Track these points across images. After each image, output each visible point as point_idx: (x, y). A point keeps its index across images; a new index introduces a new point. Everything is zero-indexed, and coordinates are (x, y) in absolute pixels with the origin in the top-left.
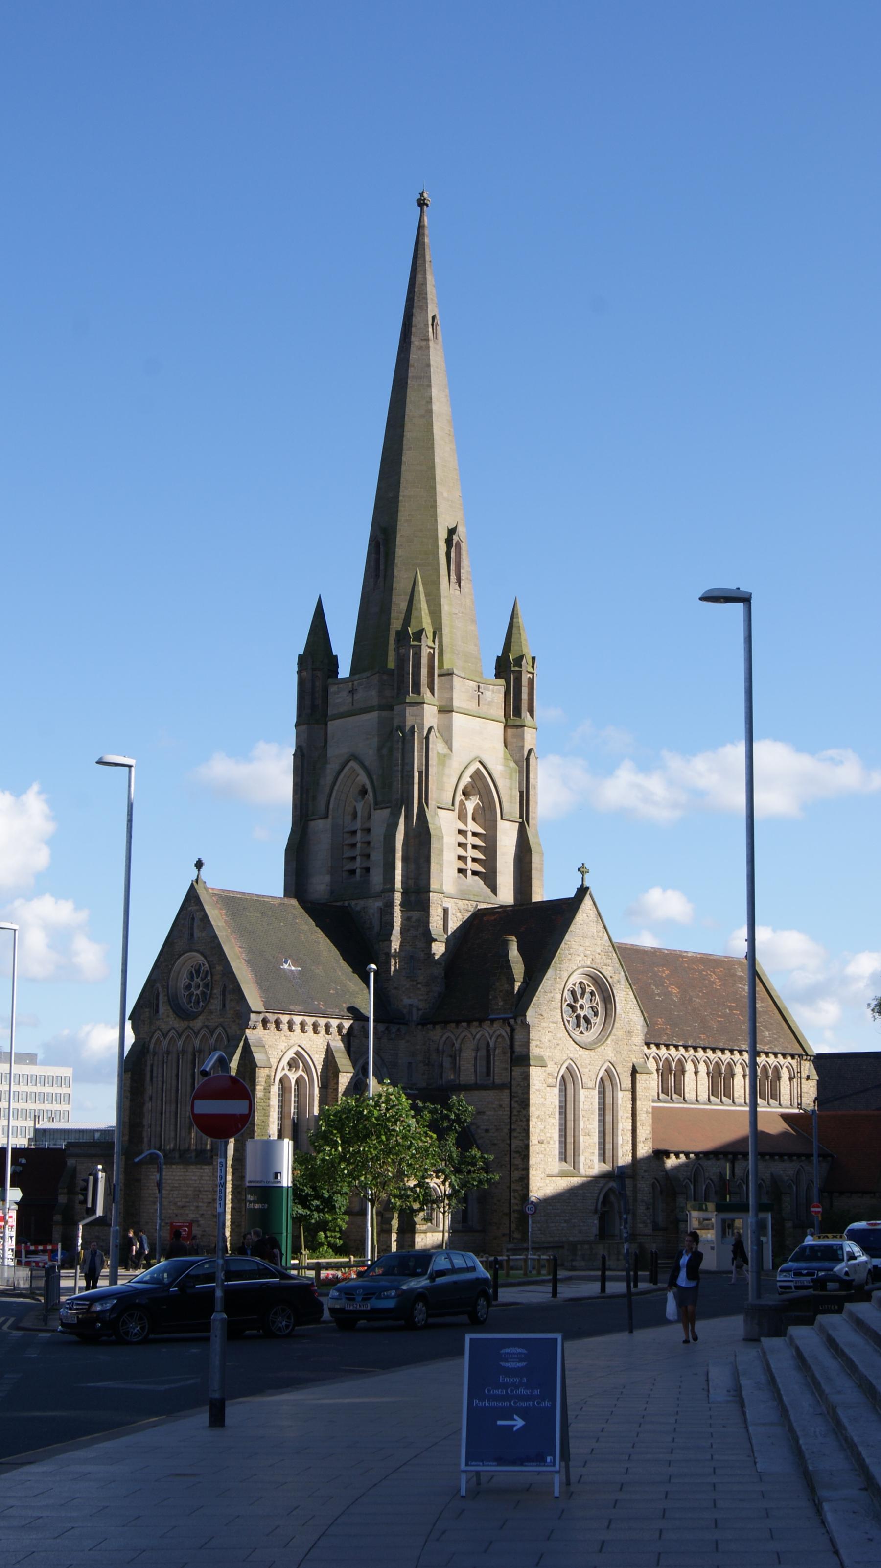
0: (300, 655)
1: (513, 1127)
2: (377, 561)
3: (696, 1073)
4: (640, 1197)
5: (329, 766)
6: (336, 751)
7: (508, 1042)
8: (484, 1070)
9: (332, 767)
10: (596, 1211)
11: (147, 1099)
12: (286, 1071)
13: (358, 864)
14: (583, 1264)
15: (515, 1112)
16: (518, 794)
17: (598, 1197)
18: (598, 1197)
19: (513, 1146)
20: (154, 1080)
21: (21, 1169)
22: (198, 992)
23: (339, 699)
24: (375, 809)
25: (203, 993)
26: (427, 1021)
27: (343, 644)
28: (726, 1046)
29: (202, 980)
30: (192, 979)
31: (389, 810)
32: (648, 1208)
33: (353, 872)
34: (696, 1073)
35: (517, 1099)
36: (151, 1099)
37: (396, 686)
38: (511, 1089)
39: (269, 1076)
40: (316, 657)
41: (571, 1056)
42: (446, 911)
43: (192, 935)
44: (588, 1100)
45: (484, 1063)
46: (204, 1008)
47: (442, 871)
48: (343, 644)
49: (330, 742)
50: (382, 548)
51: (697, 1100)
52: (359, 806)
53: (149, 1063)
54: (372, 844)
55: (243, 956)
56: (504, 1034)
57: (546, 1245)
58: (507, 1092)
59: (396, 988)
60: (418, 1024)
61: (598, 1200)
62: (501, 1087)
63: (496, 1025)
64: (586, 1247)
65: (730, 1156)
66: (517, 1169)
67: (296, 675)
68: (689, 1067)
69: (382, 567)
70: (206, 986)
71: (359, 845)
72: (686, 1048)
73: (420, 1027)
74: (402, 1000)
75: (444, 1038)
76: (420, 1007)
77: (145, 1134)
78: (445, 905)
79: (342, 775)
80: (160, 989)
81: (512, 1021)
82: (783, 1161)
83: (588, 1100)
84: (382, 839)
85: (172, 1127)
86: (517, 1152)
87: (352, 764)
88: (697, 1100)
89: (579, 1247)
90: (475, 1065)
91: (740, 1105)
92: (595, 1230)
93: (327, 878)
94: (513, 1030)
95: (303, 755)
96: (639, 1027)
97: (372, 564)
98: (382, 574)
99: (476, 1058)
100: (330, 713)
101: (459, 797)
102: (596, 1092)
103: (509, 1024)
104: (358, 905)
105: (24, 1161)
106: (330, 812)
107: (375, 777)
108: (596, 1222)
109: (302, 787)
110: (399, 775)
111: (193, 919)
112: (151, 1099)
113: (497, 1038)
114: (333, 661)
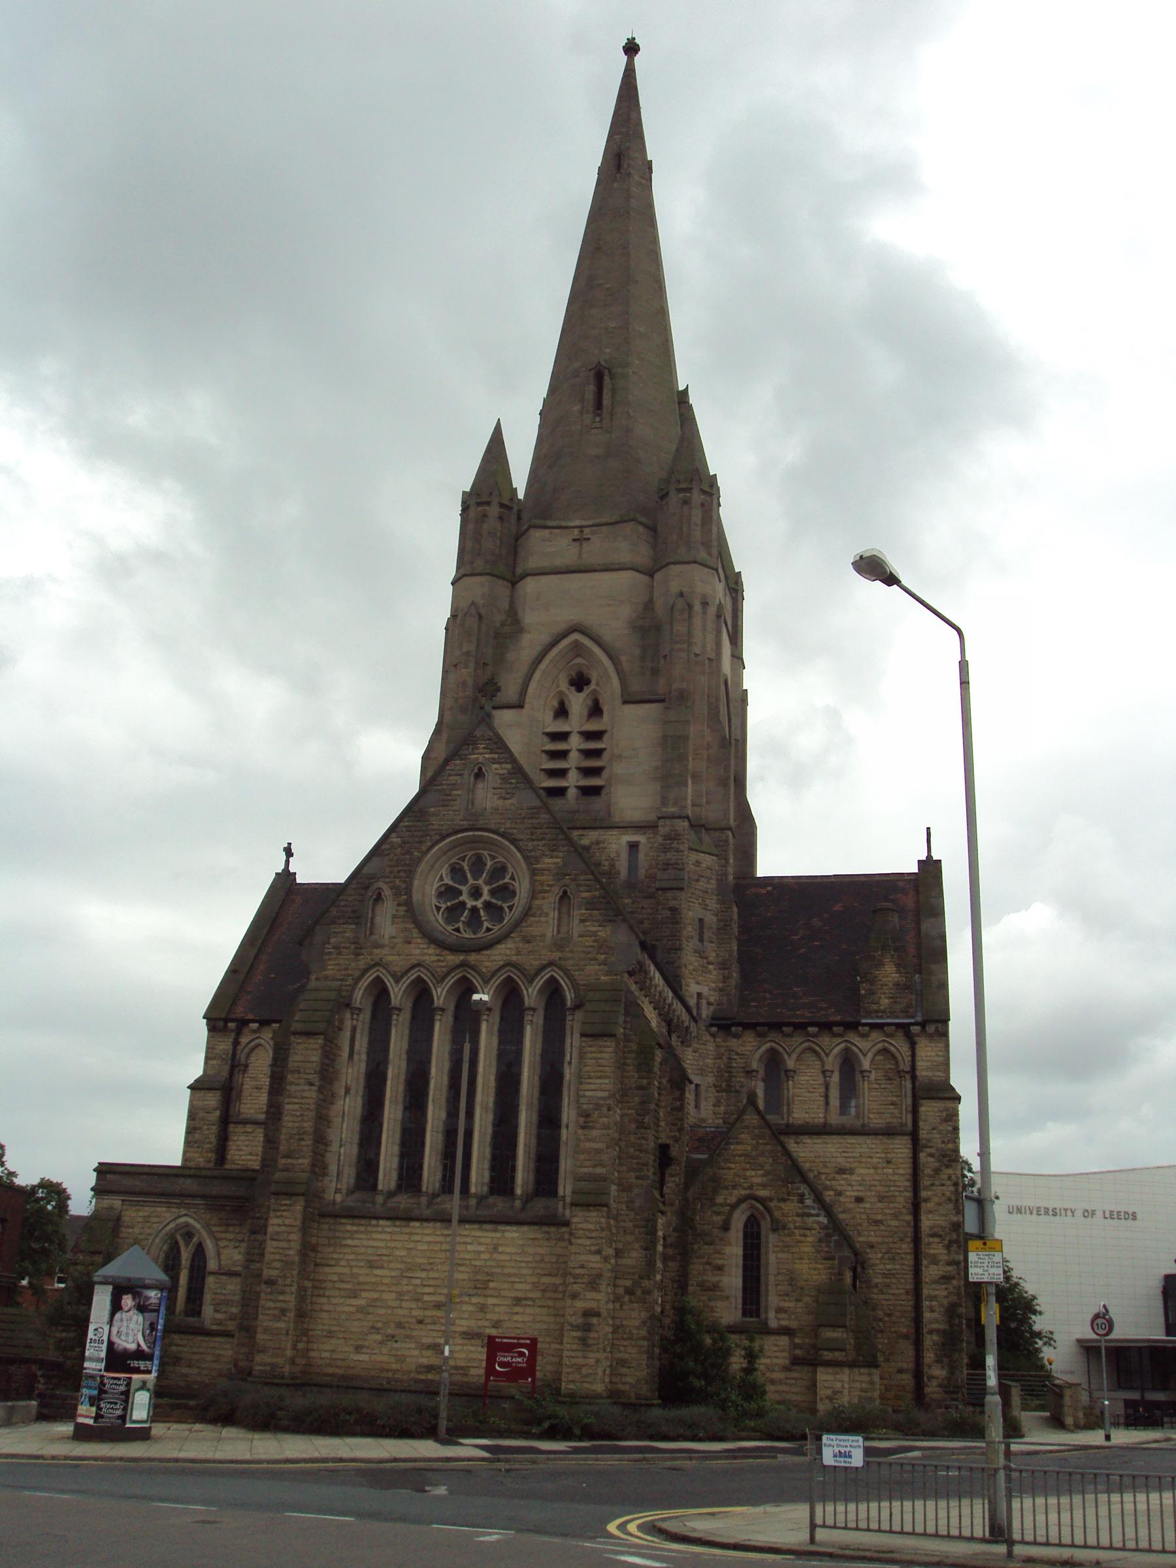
60: (712, 1025)
66: (934, 1261)
76: (712, 999)
94: (913, 1046)
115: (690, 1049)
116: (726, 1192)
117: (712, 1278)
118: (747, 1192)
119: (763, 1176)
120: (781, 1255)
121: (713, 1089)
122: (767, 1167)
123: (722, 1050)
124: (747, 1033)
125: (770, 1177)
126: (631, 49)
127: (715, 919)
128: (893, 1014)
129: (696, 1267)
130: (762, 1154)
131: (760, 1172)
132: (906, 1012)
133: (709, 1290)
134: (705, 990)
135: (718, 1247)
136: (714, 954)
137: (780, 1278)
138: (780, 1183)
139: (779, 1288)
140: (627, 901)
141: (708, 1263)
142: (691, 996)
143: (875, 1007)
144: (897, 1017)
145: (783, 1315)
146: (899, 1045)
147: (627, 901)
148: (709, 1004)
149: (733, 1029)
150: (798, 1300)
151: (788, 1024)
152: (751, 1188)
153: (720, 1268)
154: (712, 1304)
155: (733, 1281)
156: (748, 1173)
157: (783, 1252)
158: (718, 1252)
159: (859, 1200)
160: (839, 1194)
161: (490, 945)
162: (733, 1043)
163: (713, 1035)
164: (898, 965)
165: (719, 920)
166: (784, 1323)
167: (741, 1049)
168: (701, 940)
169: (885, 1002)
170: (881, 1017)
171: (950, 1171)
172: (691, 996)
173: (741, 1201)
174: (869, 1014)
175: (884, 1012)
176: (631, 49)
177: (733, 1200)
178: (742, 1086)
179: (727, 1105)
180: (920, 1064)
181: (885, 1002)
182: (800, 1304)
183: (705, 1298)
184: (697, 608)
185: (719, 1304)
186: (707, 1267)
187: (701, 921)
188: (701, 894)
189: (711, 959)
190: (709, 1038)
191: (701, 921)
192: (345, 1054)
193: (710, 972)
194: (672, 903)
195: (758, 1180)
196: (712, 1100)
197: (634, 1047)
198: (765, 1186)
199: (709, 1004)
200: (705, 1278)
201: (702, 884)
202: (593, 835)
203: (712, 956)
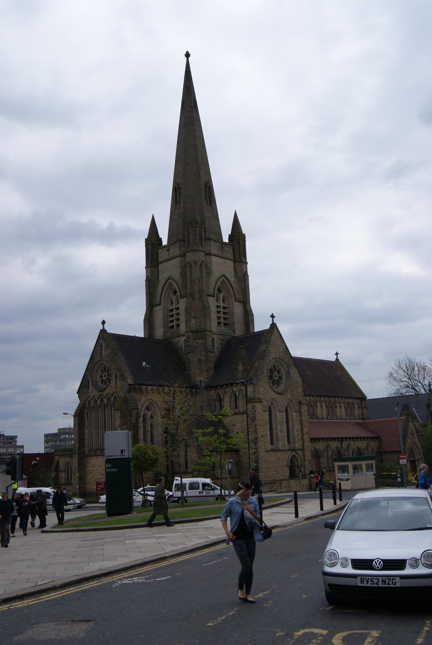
0: (146, 239)
1: (249, 430)
2: (176, 197)
3: (322, 406)
4: (306, 458)
5: (160, 283)
6: (163, 277)
7: (245, 393)
8: (234, 406)
9: (161, 283)
10: (288, 466)
11: (86, 428)
12: (146, 411)
13: (174, 323)
14: (285, 489)
15: (249, 423)
16: (241, 290)
17: (288, 459)
18: (288, 459)
19: (250, 438)
20: (89, 419)
21: (37, 462)
22: (105, 378)
23: (163, 255)
24: (181, 298)
25: (108, 379)
26: (208, 388)
27: (164, 234)
28: (333, 395)
29: (107, 373)
30: (103, 373)
31: (186, 298)
32: (310, 463)
33: (172, 327)
34: (322, 406)
35: (250, 417)
36: (88, 427)
37: (186, 245)
38: (247, 413)
39: (137, 413)
40: (153, 241)
41: (273, 397)
42: (213, 339)
43: (102, 354)
44: (280, 416)
45: (234, 403)
46: (108, 385)
47: (211, 322)
48: (164, 234)
49: (160, 273)
50: (178, 191)
51: (322, 418)
52: (174, 298)
53: (86, 412)
54: (180, 313)
55: (124, 361)
56: (243, 389)
57: (268, 482)
58: (245, 415)
59: (193, 373)
60: (204, 388)
61: (288, 461)
62: (243, 413)
63: (239, 386)
64: (286, 482)
65: (340, 439)
66: (252, 449)
67: (145, 248)
68: (319, 404)
69: (178, 199)
70: (109, 375)
71: (175, 315)
72: (317, 396)
73: (205, 389)
74: (196, 379)
75: (216, 393)
76: (205, 381)
77: (86, 443)
78: (213, 337)
79: (166, 286)
80: (89, 379)
81: (246, 383)
82: (358, 440)
83: (280, 416)
84: (184, 310)
85: (97, 439)
86: (251, 441)
87: (170, 280)
88: (322, 418)
89: (283, 482)
90: (230, 405)
91: (340, 419)
92: (288, 474)
93: (162, 330)
94: (246, 387)
95: (149, 280)
96: (301, 384)
97: (174, 198)
98: (178, 202)
99: (230, 401)
100: (159, 261)
101: (216, 292)
102: (285, 413)
103: (244, 384)
104: (175, 340)
105: (38, 459)
106: (162, 302)
107: (180, 285)
108: (288, 470)
109: (149, 293)
110: (189, 282)
111: (102, 347)
112: (88, 427)
113: (240, 391)
114: (160, 240)
126: (187, 55)
127: (204, 358)
128: (242, 379)
132: (245, 378)
134: (202, 379)
143: (238, 377)
146: (243, 388)
148: (204, 382)
151: (209, 387)
159: (238, 433)
160: (233, 432)
161: (105, 390)
163: (206, 391)
164: (242, 365)
168: (200, 364)
169: (240, 376)
171: (254, 423)
172: (198, 381)
173: (182, 440)
174: (237, 380)
176: (187, 55)
180: (248, 393)
181: (240, 376)
184: (193, 265)
187: (200, 359)
189: (204, 369)
191: (200, 359)
192: (86, 419)
193: (204, 373)
195: (185, 435)
197: (128, 410)
202: (177, 339)
203: (204, 369)
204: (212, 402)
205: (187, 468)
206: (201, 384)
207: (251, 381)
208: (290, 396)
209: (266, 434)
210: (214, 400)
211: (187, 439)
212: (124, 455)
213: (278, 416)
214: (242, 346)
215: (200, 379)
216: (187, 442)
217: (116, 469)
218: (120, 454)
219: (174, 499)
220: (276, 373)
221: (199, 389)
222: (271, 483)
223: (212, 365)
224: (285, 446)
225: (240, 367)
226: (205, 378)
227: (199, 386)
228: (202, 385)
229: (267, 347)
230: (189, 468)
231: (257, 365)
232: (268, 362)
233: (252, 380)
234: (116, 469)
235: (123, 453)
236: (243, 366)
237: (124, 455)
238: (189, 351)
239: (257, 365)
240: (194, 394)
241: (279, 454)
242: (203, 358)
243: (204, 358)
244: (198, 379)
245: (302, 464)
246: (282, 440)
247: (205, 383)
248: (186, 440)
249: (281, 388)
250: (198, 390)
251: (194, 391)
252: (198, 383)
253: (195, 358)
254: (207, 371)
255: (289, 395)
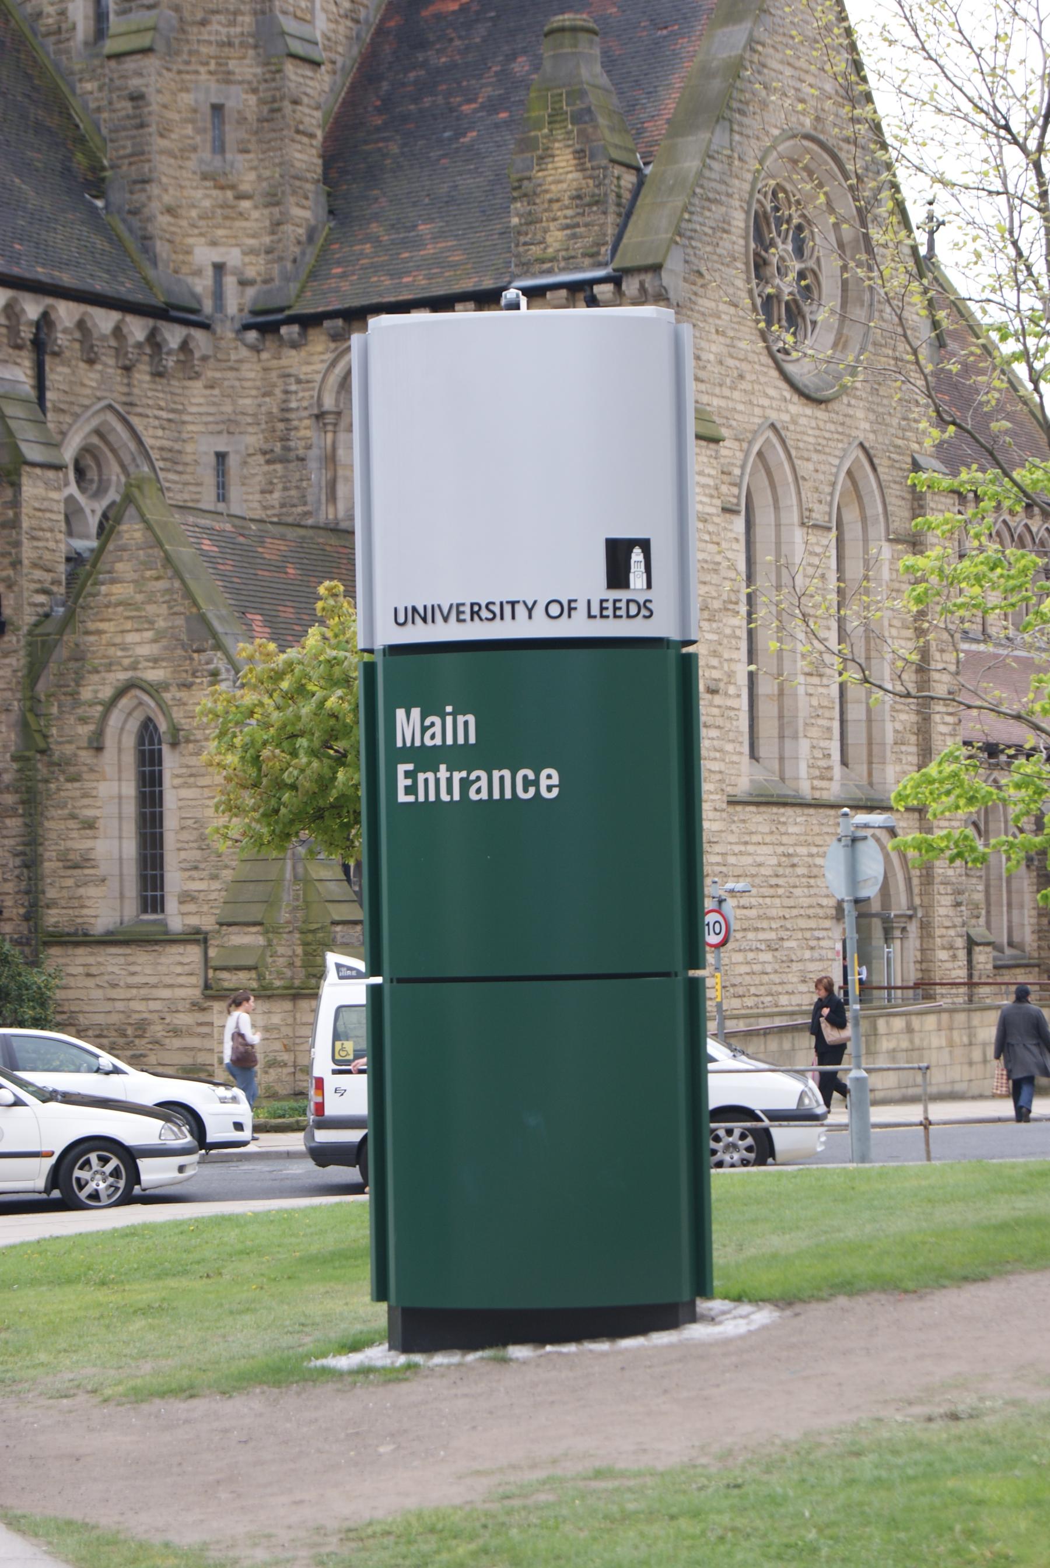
26: (267, 324)
41: (773, 416)
59: (170, 210)
60: (247, 327)
73: (252, 335)
76: (251, 273)
115: (198, 384)
116: (95, 678)
117: (80, 844)
118: (129, 674)
119: (155, 641)
120: (185, 793)
121: (261, 459)
122: (161, 624)
123: (274, 375)
124: (313, 334)
125: (164, 642)
127: (252, 100)
128: (570, 262)
129: (54, 825)
130: (150, 601)
131: (149, 635)
133: (76, 867)
134: (233, 257)
135: (88, 785)
136: (252, 176)
137: (185, 836)
138: (180, 652)
139: (183, 855)
140: (89, 86)
141: (73, 817)
142: (198, 273)
143: (535, 251)
144: (578, 269)
145: (191, 907)
147: (89, 86)
148: (243, 283)
149: (284, 330)
150: (214, 877)
151: (290, 320)
152: (134, 667)
153: (90, 825)
154: (82, 891)
155: (115, 846)
156: (130, 638)
157: (186, 785)
158: (85, 796)
162: (292, 359)
163: (256, 349)
164: (579, 154)
165: (262, 102)
166: (194, 921)
167: (304, 371)
168: (219, 147)
169: (556, 238)
170: (550, 272)
172: (198, 273)
173: (121, 693)
175: (552, 260)
177: (106, 693)
178: (309, 447)
179: (285, 489)
181: (556, 238)
182: (216, 885)
183: (70, 882)
185: (91, 891)
186: (72, 824)
187: (217, 109)
188: (212, 50)
189: (245, 187)
190: (244, 352)
191: (217, 109)
194: (135, 82)
195: (144, 650)
196: (258, 481)
198: (155, 660)
199: (243, 283)
200: (70, 844)
201: (218, 28)
203: (248, 181)
204: (306, 430)
205: (152, 897)
206: (218, 294)
207: (648, 278)
208: (863, 428)
209: (731, 674)
210: (320, 416)
211: (165, 686)
212: (646, 609)
213: (799, 549)
214: (580, 19)
215: (215, 255)
216: (161, 705)
217: (549, 780)
218: (591, 580)
219: (323, 1136)
220: (784, 248)
221: (205, 326)
222: (782, 1030)
223: (306, 157)
224: (825, 775)
225: (561, 173)
226: (252, 252)
227: (208, 306)
228: (232, 307)
229: (752, 43)
230: (171, 905)
231: (691, 165)
232: (752, 150)
233: (656, 268)
234: (549, 780)
235: (637, 579)
236: (581, 168)
237: (646, 609)
238: (145, 40)
239: (691, 165)
240: (170, 362)
241: (795, 821)
242: (242, 101)
243: (252, 100)
244: (204, 255)
245: (912, 907)
246: (814, 732)
247: (251, 292)
248: (154, 690)
249: (812, 355)
250: (198, 334)
251: (173, 336)
252: (202, 285)
253: (187, 99)
254: (273, 199)
255: (860, 414)
